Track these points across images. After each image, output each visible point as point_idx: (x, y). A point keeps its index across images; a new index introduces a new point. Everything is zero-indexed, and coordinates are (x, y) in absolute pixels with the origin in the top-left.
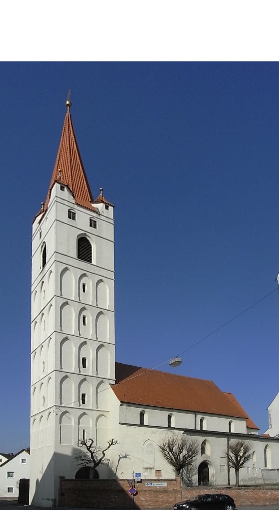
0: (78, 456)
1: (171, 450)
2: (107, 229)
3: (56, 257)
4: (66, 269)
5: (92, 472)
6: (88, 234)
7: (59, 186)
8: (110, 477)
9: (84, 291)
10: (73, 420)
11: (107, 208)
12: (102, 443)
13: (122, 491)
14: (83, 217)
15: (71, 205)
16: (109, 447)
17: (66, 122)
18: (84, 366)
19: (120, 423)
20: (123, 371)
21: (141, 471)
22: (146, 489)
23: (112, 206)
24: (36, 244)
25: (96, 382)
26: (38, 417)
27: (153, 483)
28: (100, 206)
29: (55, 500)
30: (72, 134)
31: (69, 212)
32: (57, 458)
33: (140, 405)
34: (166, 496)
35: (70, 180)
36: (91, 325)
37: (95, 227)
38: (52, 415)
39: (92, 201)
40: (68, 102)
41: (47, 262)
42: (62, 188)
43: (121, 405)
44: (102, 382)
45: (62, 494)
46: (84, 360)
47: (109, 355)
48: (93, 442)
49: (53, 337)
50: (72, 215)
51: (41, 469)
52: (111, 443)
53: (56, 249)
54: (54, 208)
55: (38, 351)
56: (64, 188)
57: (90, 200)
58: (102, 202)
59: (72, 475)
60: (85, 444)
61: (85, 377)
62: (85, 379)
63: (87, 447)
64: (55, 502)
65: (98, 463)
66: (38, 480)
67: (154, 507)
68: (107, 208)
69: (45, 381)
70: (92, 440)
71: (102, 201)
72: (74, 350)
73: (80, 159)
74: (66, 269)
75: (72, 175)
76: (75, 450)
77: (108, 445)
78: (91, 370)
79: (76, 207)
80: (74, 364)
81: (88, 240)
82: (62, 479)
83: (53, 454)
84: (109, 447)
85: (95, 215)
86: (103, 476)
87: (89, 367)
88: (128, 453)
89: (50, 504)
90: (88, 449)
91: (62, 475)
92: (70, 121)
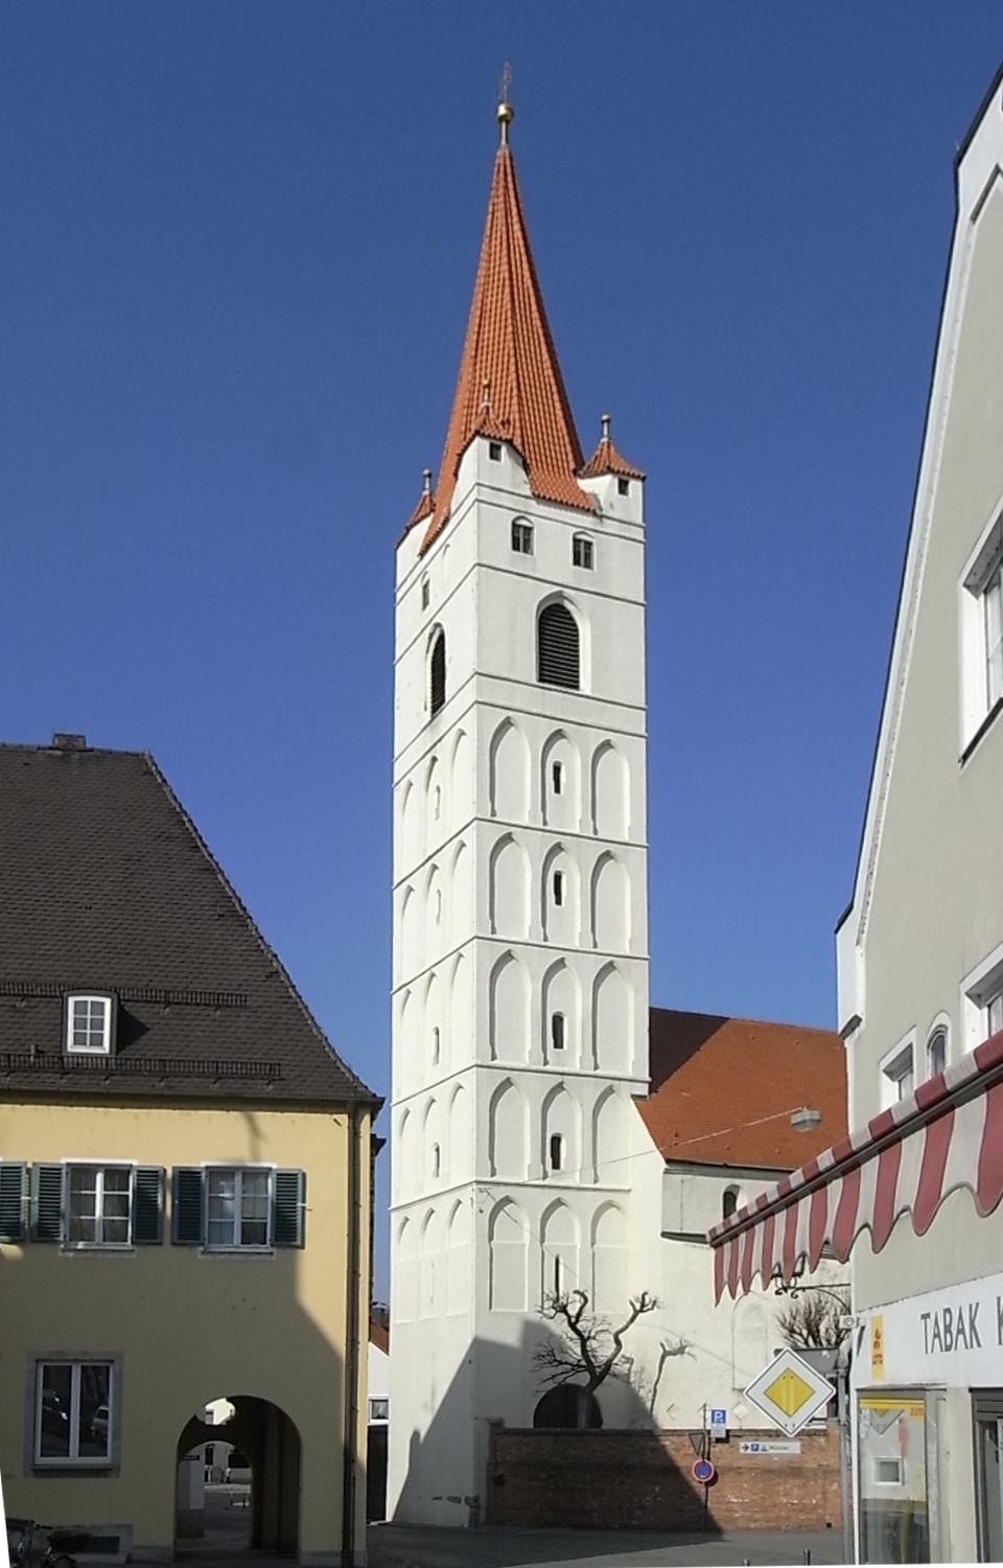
0: (540, 1347)
1: (814, 1332)
2: (623, 565)
3: (479, 688)
4: (507, 724)
5: (583, 1404)
6: (567, 592)
7: (486, 444)
8: (633, 1422)
9: (557, 790)
10: (527, 1226)
11: (623, 488)
12: (609, 1309)
13: (672, 1471)
14: (554, 531)
15: (521, 504)
16: (633, 1319)
17: (497, 181)
18: (558, 1044)
19: (664, 1235)
20: (675, 1038)
21: (723, 1401)
22: (741, 1464)
23: (638, 478)
24: (409, 624)
25: (592, 1091)
26: (417, 1215)
27: (761, 1444)
28: (600, 487)
29: (476, 1500)
30: (517, 227)
31: (515, 527)
32: (481, 1353)
33: (725, 1166)
34: (799, 1487)
35: (515, 408)
36: (578, 902)
37: (588, 565)
38: (467, 1213)
39: (581, 468)
40: (502, 110)
41: (448, 697)
42: (494, 454)
43: (667, 1172)
44: (610, 1091)
45: (496, 1482)
46: (558, 1020)
47: (631, 994)
48: (586, 1300)
49: (470, 952)
50: (521, 538)
51: (429, 1400)
52: (638, 1306)
53: (479, 662)
54: (470, 522)
55: (417, 988)
56: (499, 448)
57: (572, 466)
58: (610, 470)
59: (522, 1417)
60: (564, 1310)
61: (559, 1079)
62: (560, 1087)
63: (569, 1317)
64: (478, 1507)
65: (600, 1373)
66: (416, 1434)
67: (764, 1525)
68: (623, 488)
69: (443, 1093)
70: (582, 1295)
71: (609, 468)
72: (530, 990)
73: (543, 318)
74: (507, 724)
75: (511, 279)
76: (530, 1329)
77: (632, 1312)
78: (579, 1054)
79: (534, 507)
80: (528, 1038)
81: (568, 612)
82: (497, 1430)
83: (470, 1341)
84: (633, 1319)
85: (587, 521)
86: (612, 1420)
87: (572, 1045)
88: (689, 1338)
89: (460, 1515)
90: (573, 1326)
91: (495, 1414)
92: (510, 178)
